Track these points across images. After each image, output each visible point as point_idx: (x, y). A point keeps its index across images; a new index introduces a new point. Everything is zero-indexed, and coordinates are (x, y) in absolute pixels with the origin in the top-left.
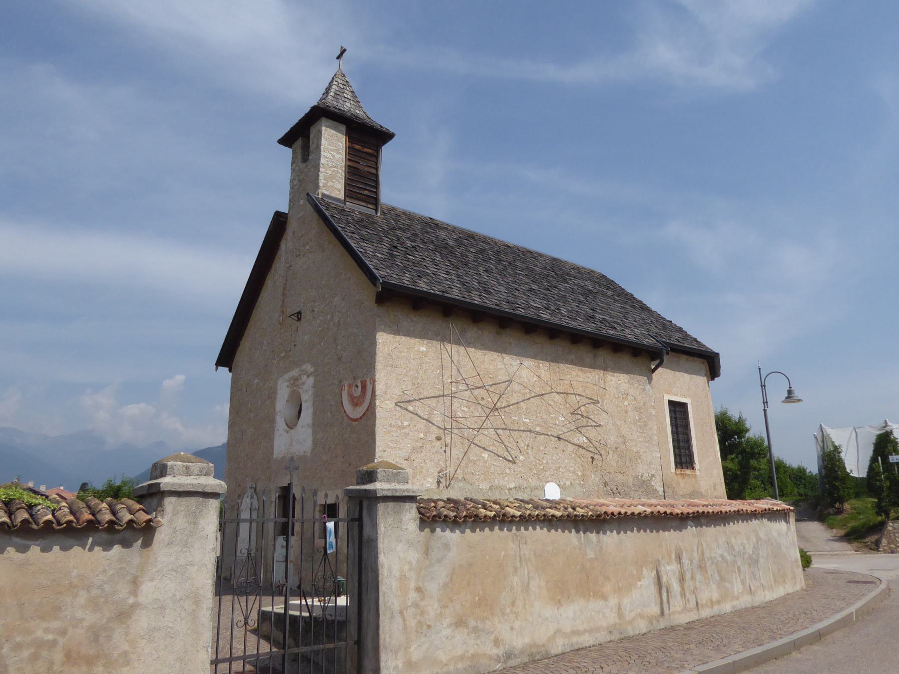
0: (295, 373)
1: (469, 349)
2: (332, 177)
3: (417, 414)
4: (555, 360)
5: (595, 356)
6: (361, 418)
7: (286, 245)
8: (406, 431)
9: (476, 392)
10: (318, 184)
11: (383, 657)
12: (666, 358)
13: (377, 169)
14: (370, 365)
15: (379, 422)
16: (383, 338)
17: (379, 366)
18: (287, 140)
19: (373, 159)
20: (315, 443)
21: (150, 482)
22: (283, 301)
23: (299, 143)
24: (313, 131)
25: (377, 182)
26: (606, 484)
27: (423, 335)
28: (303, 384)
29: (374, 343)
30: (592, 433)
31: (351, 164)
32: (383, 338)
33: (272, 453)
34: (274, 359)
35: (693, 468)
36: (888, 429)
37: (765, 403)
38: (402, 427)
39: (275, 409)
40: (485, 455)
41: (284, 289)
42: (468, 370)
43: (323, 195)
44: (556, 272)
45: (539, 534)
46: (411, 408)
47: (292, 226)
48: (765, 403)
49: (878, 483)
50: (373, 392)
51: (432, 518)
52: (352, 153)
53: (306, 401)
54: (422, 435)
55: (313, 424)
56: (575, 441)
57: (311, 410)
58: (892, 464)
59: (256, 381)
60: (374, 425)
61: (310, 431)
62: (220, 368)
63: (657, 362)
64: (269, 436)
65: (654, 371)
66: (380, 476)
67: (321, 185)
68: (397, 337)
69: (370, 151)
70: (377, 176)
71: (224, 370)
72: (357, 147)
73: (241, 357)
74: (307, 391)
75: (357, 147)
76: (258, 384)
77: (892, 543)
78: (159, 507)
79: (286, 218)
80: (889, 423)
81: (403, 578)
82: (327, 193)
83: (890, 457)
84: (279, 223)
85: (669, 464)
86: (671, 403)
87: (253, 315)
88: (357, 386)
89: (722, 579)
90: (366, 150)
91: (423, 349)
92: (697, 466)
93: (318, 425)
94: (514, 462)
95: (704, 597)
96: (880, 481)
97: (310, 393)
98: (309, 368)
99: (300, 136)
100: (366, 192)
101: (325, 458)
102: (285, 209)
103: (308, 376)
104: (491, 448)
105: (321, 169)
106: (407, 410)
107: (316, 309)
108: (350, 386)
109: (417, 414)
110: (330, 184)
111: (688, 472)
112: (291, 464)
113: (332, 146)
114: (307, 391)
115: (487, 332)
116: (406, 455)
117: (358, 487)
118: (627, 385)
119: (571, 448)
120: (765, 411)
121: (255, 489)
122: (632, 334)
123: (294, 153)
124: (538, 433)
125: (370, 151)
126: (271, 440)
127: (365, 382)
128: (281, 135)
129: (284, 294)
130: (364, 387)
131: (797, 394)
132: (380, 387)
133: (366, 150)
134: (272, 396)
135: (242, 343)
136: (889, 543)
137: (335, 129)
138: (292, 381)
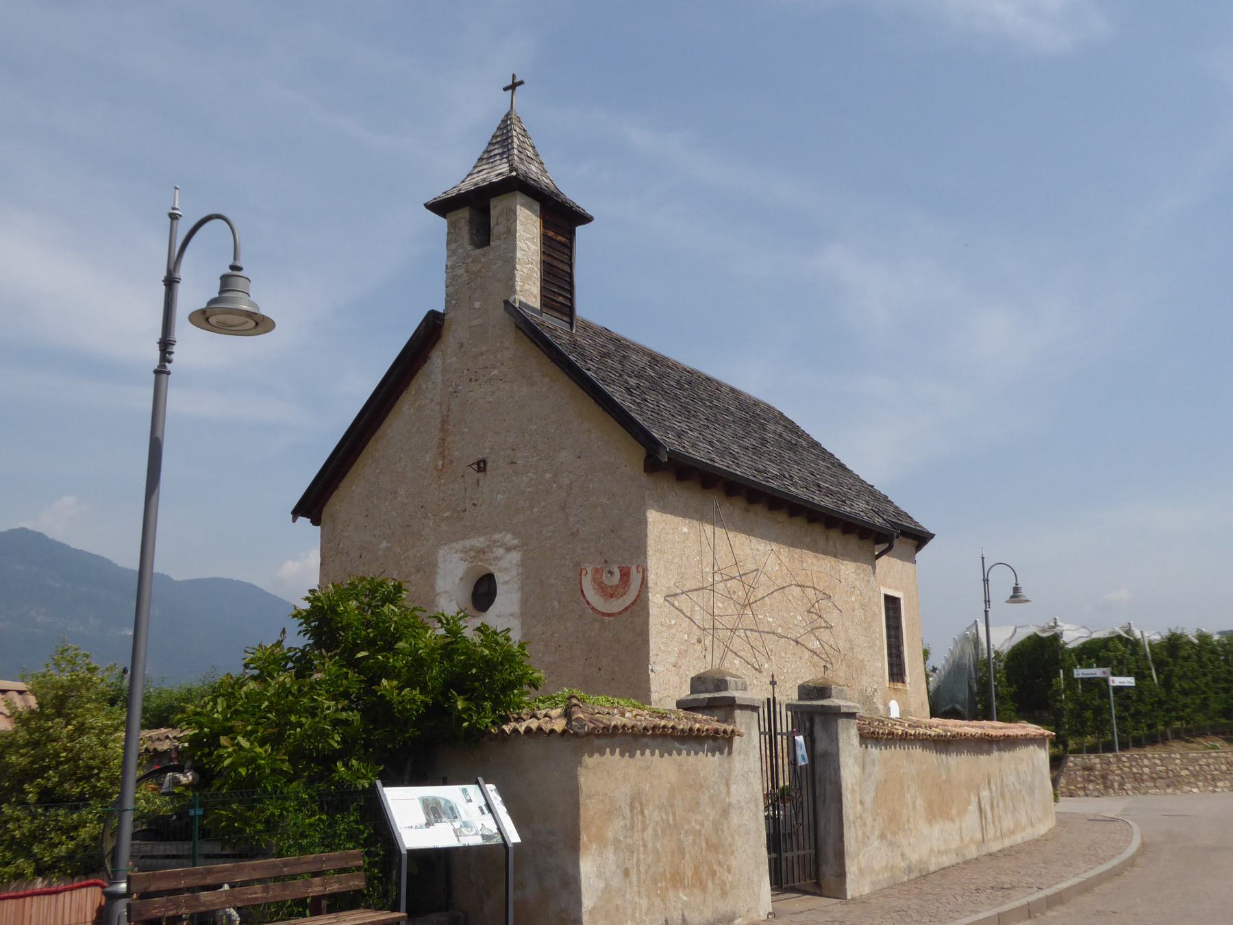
0: (479, 542)
1: (731, 535)
2: (527, 278)
3: (681, 611)
4: (793, 544)
5: (827, 539)
6: (620, 613)
7: (438, 361)
8: (673, 631)
9: (729, 584)
10: (513, 286)
11: (848, 862)
12: (896, 542)
13: (571, 266)
14: (639, 548)
15: (652, 620)
16: (653, 516)
17: (650, 551)
19: (567, 251)
21: (711, 695)
22: (443, 439)
25: (571, 284)
27: (684, 514)
28: (498, 559)
29: (643, 522)
30: (825, 635)
31: (549, 260)
32: (653, 516)
35: (903, 682)
36: (1057, 630)
37: (987, 602)
38: (670, 627)
39: (433, 587)
40: (737, 662)
41: (444, 422)
42: (724, 560)
43: (520, 302)
44: (755, 417)
45: (917, 752)
46: (676, 604)
48: (987, 602)
49: (1058, 705)
51: (869, 737)
52: (546, 241)
53: (506, 583)
54: (686, 637)
56: (810, 645)
57: (516, 596)
58: (1076, 680)
59: (384, 545)
60: (647, 623)
62: (300, 519)
63: (883, 547)
65: (878, 557)
66: (833, 692)
67: (518, 288)
69: (563, 239)
70: (571, 275)
71: (304, 521)
72: (551, 234)
74: (506, 570)
75: (551, 234)
76: (388, 549)
77: (1072, 784)
78: (729, 718)
79: (443, 321)
80: (1059, 623)
81: (853, 791)
82: (524, 300)
83: (1075, 672)
84: (431, 330)
85: (883, 677)
86: (887, 598)
88: (611, 573)
89: (1015, 808)
90: (559, 238)
91: (685, 530)
92: (907, 679)
94: (760, 671)
95: (1008, 823)
96: (1061, 701)
97: (515, 573)
98: (509, 539)
99: (472, 212)
100: (560, 299)
102: (440, 308)
103: (508, 550)
104: (742, 654)
105: (518, 267)
107: (520, 462)
108: (596, 571)
110: (527, 287)
111: (900, 685)
113: (527, 229)
114: (506, 570)
115: (736, 508)
116: (673, 660)
117: (809, 703)
118: (854, 576)
119: (807, 654)
120: (986, 612)
122: (859, 508)
123: (452, 226)
124: (780, 636)
127: (629, 569)
128: (429, 199)
129: (443, 430)
130: (625, 575)
131: (1025, 592)
133: (559, 238)
136: (1068, 784)
138: (472, 553)
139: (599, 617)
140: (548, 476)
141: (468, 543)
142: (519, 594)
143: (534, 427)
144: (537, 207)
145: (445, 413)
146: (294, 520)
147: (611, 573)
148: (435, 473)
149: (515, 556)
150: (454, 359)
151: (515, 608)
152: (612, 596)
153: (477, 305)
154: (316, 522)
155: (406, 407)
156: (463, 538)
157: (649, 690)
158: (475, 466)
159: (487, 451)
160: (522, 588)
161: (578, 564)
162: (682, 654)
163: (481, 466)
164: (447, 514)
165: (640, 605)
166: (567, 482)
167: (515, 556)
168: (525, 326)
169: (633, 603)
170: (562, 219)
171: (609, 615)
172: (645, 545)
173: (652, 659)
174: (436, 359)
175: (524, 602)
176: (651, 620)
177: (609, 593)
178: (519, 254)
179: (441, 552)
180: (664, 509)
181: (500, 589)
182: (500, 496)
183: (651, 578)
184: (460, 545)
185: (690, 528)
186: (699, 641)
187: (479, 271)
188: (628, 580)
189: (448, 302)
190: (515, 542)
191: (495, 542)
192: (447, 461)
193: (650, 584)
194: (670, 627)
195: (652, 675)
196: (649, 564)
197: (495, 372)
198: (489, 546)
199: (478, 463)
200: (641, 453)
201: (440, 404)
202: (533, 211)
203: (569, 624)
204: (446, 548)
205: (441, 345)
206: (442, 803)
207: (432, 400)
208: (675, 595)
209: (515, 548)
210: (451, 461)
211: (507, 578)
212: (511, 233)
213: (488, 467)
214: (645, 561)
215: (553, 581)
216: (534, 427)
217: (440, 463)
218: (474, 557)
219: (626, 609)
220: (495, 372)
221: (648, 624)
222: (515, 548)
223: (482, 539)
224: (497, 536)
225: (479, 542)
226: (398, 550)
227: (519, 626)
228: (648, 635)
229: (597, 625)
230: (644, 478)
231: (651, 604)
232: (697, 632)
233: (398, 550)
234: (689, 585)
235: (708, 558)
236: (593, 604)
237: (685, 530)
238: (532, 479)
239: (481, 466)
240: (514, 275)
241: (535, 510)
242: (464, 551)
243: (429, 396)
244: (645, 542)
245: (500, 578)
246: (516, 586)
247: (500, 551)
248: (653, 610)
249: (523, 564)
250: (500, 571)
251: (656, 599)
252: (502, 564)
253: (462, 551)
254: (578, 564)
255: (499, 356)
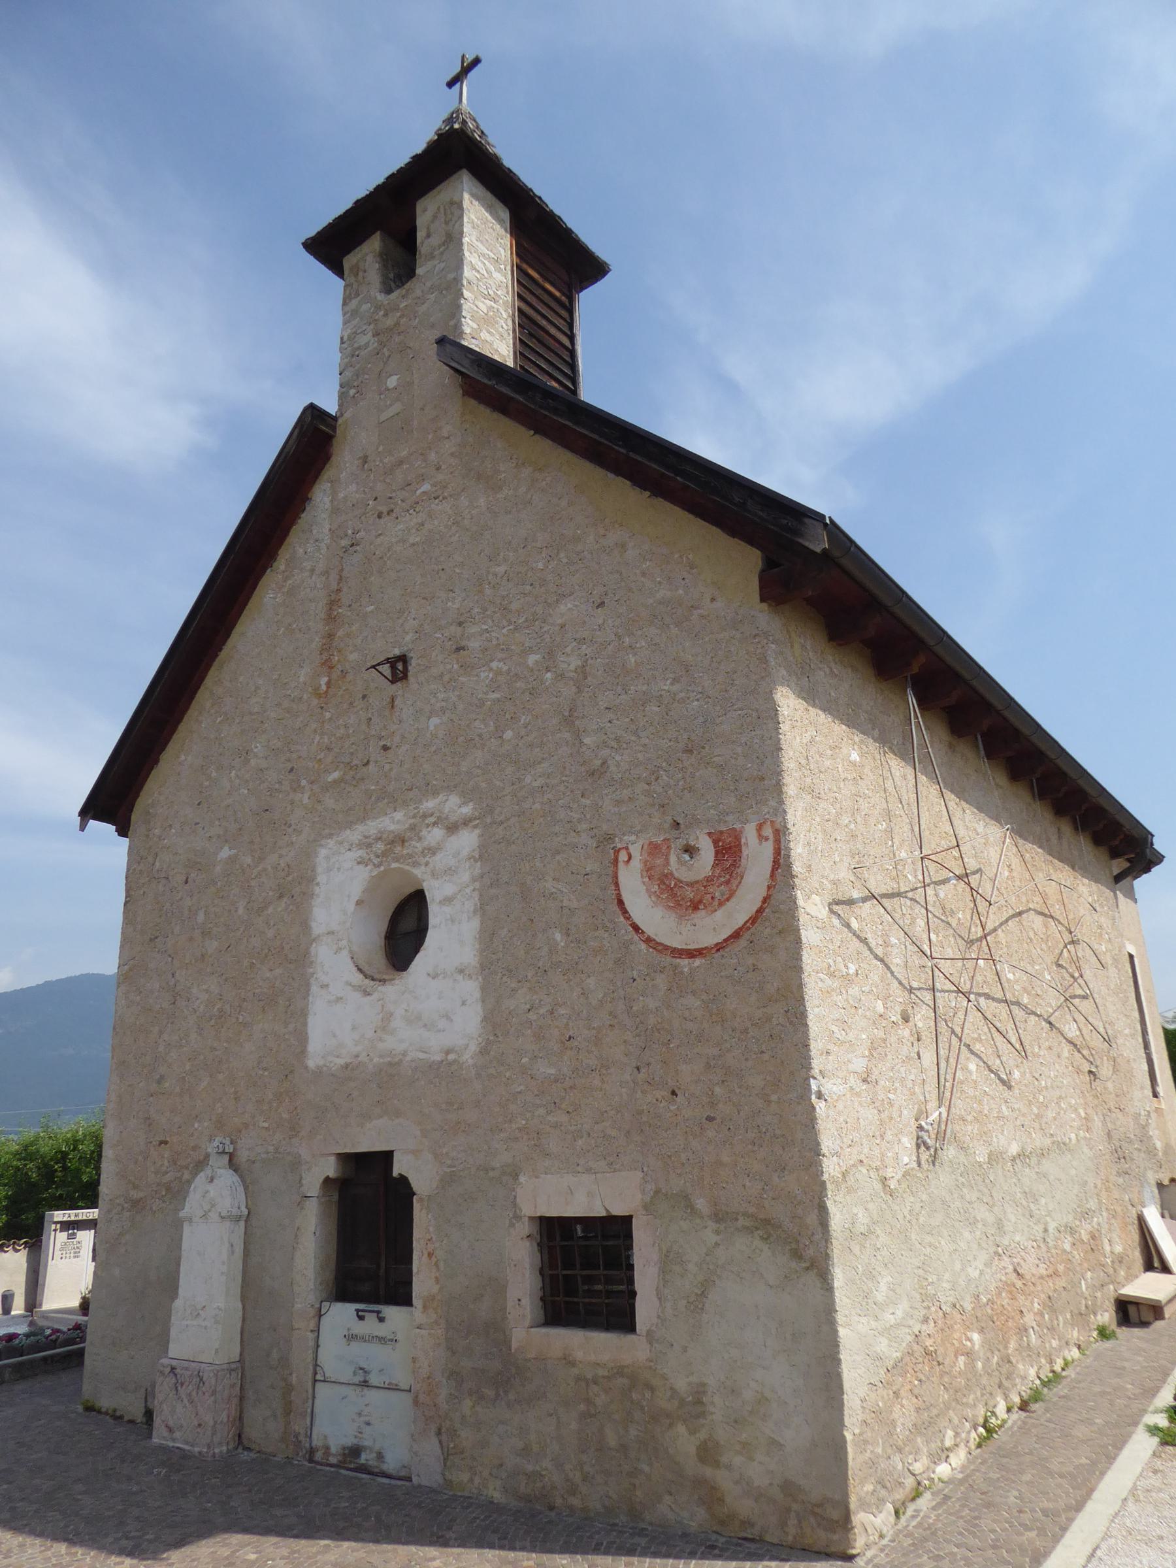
0: (393, 821)
2: (488, 321)
3: (864, 941)
6: (719, 947)
8: (854, 991)
18: (331, 246)
20: (496, 1023)
22: (330, 636)
23: (368, 255)
24: (427, 211)
26: (1109, 1135)
28: (432, 851)
33: (303, 1052)
34: (297, 788)
38: (848, 979)
39: (305, 926)
41: (332, 604)
46: (855, 924)
47: (344, 460)
50: (780, 863)
53: (448, 900)
55: (483, 967)
57: (470, 927)
59: (225, 853)
60: (795, 966)
61: (471, 988)
64: (288, 997)
68: (813, 711)
69: (558, 294)
70: (572, 353)
71: (102, 829)
73: (165, 789)
74: (450, 871)
76: (232, 860)
79: (334, 428)
84: (312, 442)
87: (209, 681)
88: (690, 850)
93: (495, 967)
97: (465, 877)
98: (454, 805)
99: (380, 232)
101: (545, 1069)
103: (452, 829)
105: (466, 293)
106: (848, 926)
107: (474, 644)
108: (654, 849)
109: (864, 941)
112: (387, 1081)
114: (450, 871)
116: (859, 1064)
119: (1066, 1050)
121: (231, 1156)
125: (558, 294)
126: (297, 1016)
127: (737, 835)
130: (728, 851)
132: (800, 850)
134: (296, 888)
135: (167, 757)
137: (489, 208)
138: (380, 847)
139: (667, 960)
140: (532, 659)
141: (372, 827)
142: (476, 923)
143: (501, 569)
144: (506, 215)
145: (335, 586)
146: (83, 827)
147: (690, 850)
148: (315, 702)
149: (467, 840)
150: (353, 487)
151: (468, 955)
152: (695, 906)
153: (392, 382)
154: (123, 831)
155: (269, 596)
156: (363, 819)
157: (815, 1150)
158: (386, 669)
159: (408, 638)
160: (482, 909)
161: (609, 838)
162: (876, 1049)
163: (398, 668)
164: (336, 775)
165: (775, 919)
166: (575, 662)
167: (467, 840)
168: (479, 380)
169: (753, 920)
170: (555, 260)
171: (691, 954)
172: (777, 773)
173: (817, 1064)
174: (322, 497)
175: (487, 937)
176: (807, 958)
177: (687, 900)
178: (467, 273)
179: (323, 852)
180: (810, 695)
181: (436, 915)
182: (435, 721)
183: (798, 851)
184: (354, 835)
185: (861, 756)
186: (906, 1019)
187: (397, 324)
188: (735, 865)
189: (342, 396)
190: (467, 810)
191: (425, 816)
192: (336, 674)
193: (797, 868)
194: (848, 979)
195: (820, 1106)
196: (790, 817)
197: (426, 487)
198: (413, 828)
199: (393, 662)
200: (742, 564)
201: (326, 573)
202: (500, 221)
203: (591, 982)
204: (331, 843)
205: (329, 473)
206: (982, 753)
207: (312, 571)
208: (850, 902)
209: (466, 822)
210: (344, 673)
211: (449, 889)
212: (453, 240)
213: (397, 652)
214: (780, 810)
215: (549, 885)
216: (501, 569)
217: (324, 680)
218: (384, 854)
219: (736, 935)
220: (426, 487)
221: (799, 969)
222: (466, 822)
223: (399, 815)
224: (429, 804)
225: (393, 821)
226: (249, 860)
227: (477, 994)
228: (801, 1000)
229: (661, 981)
230: (764, 617)
231: (803, 919)
232: (900, 996)
233: (249, 860)
234: (879, 883)
235: (903, 830)
236: (650, 931)
237: (855, 756)
238: (499, 672)
239: (398, 668)
240: (459, 307)
241: (508, 734)
242: (365, 844)
243: (307, 565)
244: (777, 763)
245: (435, 892)
246: (469, 906)
247: (437, 833)
248: (809, 936)
249: (483, 854)
250: (434, 875)
251: (811, 907)
252: (439, 861)
253: (360, 845)
254: (609, 838)
255: (432, 456)
